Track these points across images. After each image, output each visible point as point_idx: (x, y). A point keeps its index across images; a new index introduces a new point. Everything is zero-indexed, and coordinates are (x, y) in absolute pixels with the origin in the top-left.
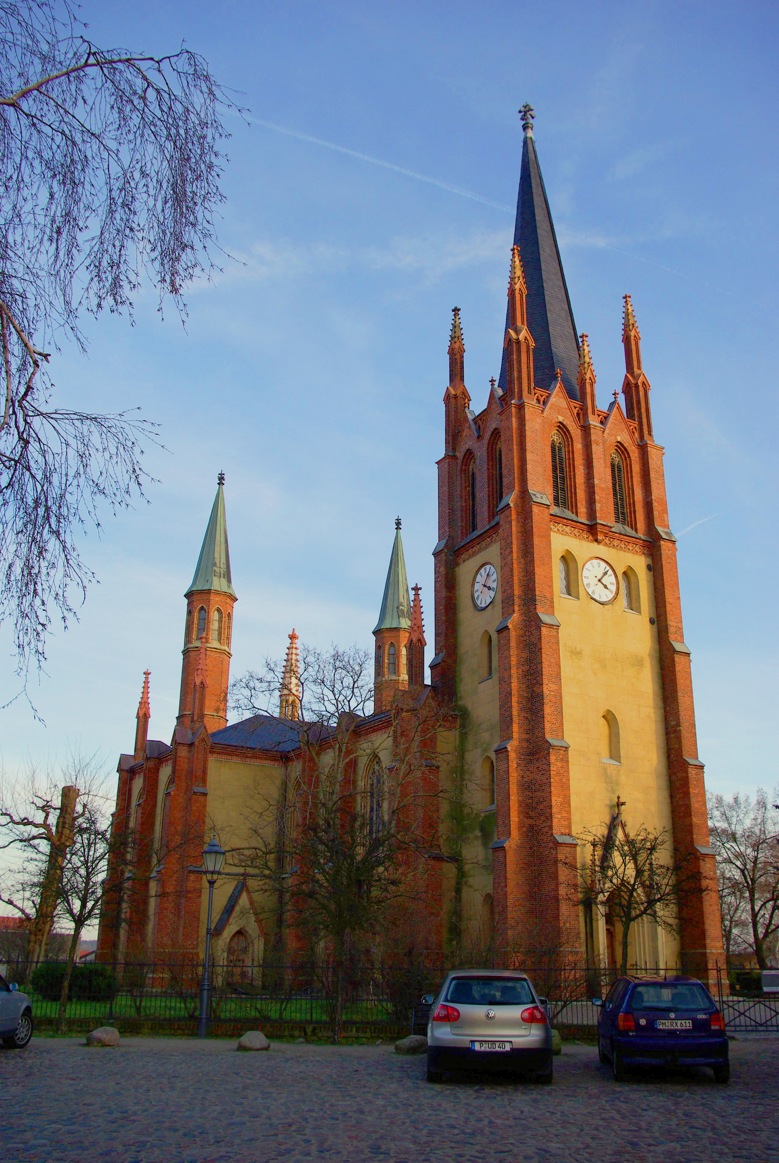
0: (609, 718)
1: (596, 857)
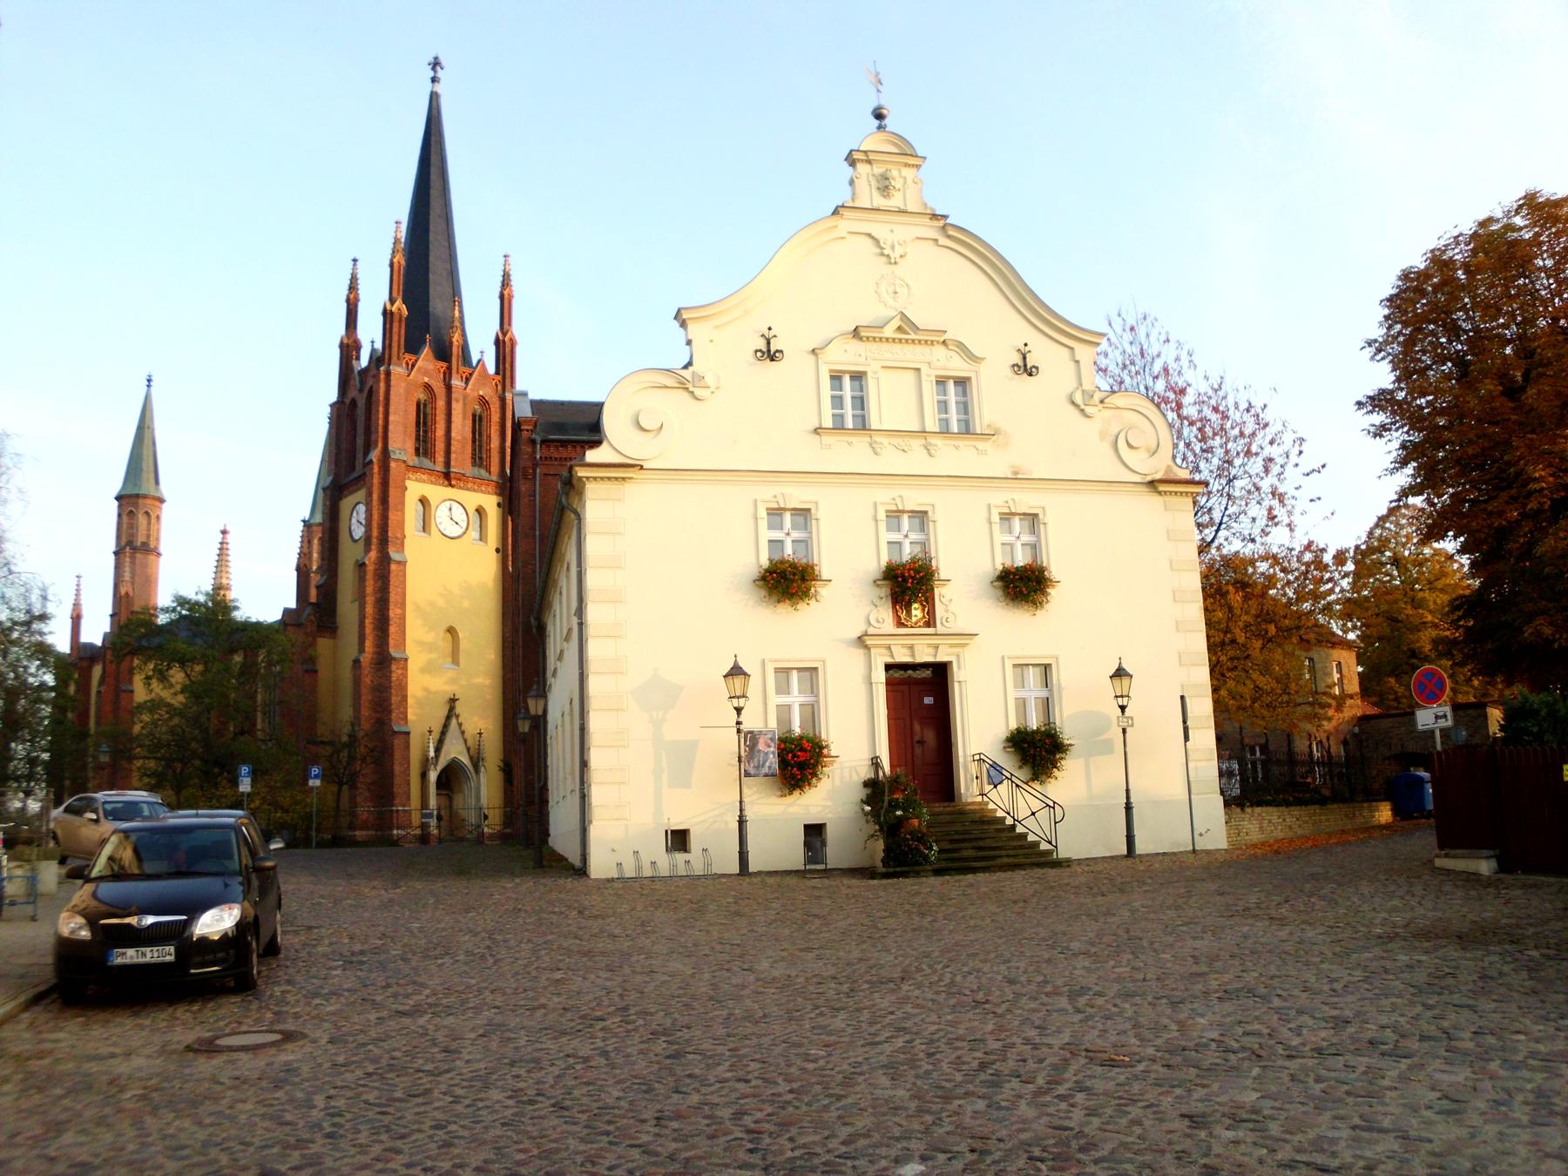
0: (451, 631)
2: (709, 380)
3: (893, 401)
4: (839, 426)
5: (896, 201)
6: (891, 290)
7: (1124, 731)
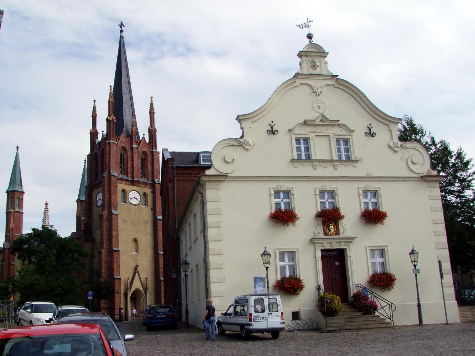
0: (135, 240)
1: (128, 282)
2: (250, 142)
3: (320, 149)
4: (299, 159)
5: (318, 71)
6: (317, 105)
7: (416, 275)
